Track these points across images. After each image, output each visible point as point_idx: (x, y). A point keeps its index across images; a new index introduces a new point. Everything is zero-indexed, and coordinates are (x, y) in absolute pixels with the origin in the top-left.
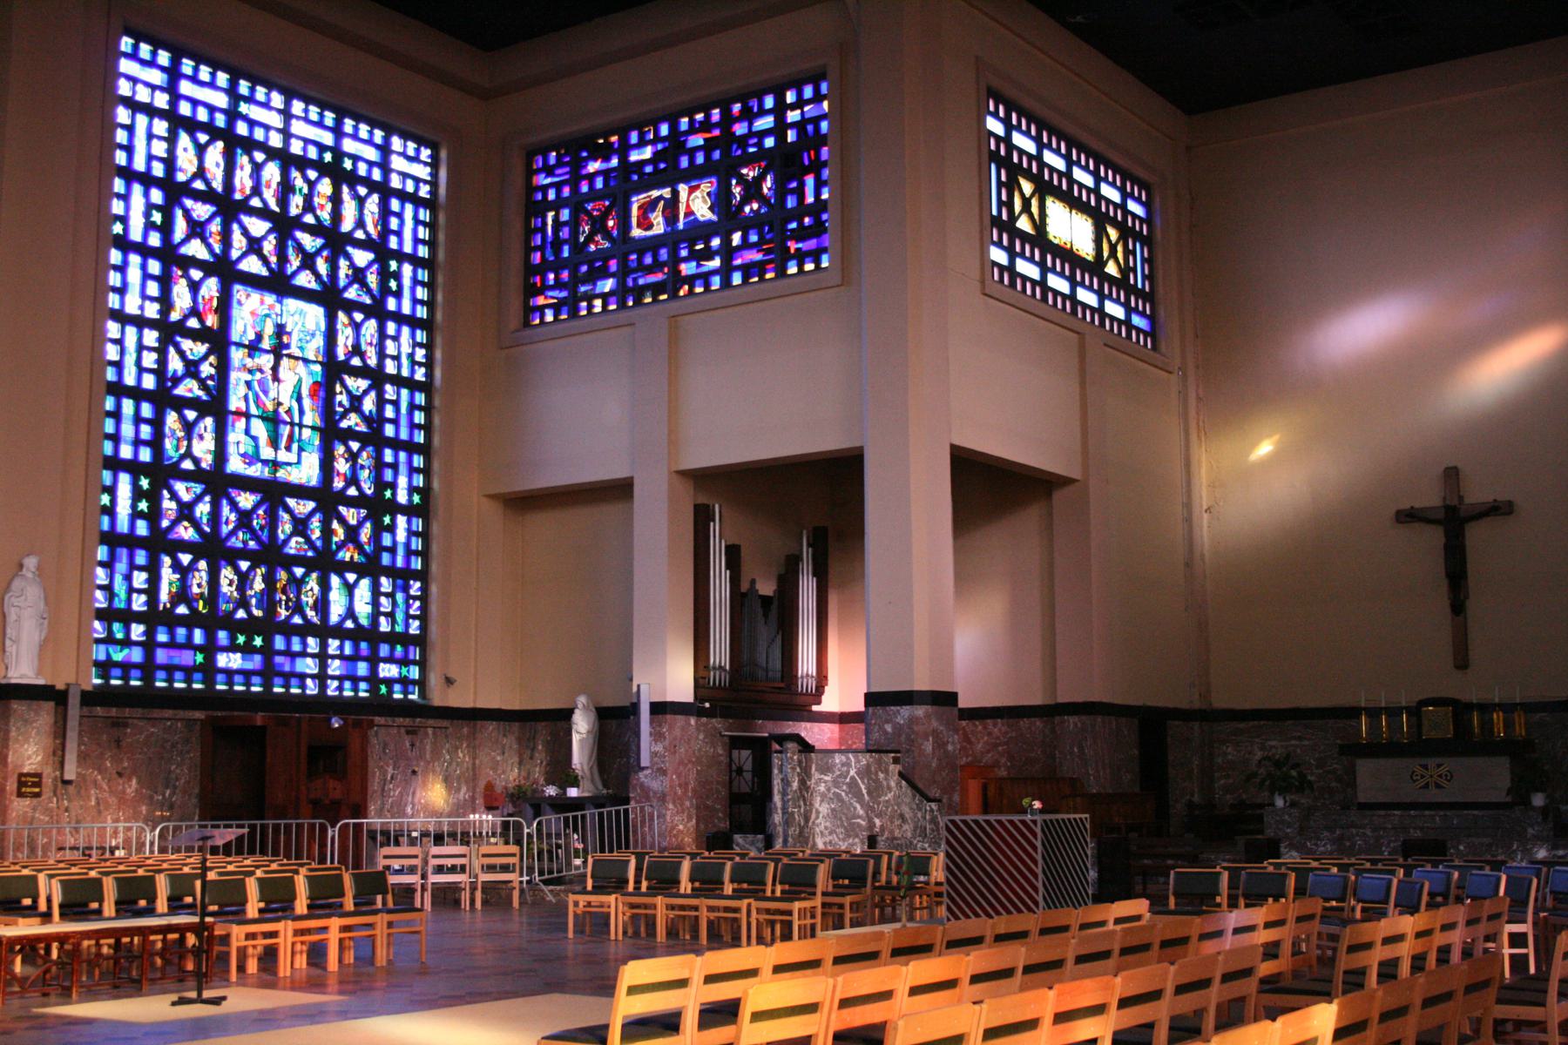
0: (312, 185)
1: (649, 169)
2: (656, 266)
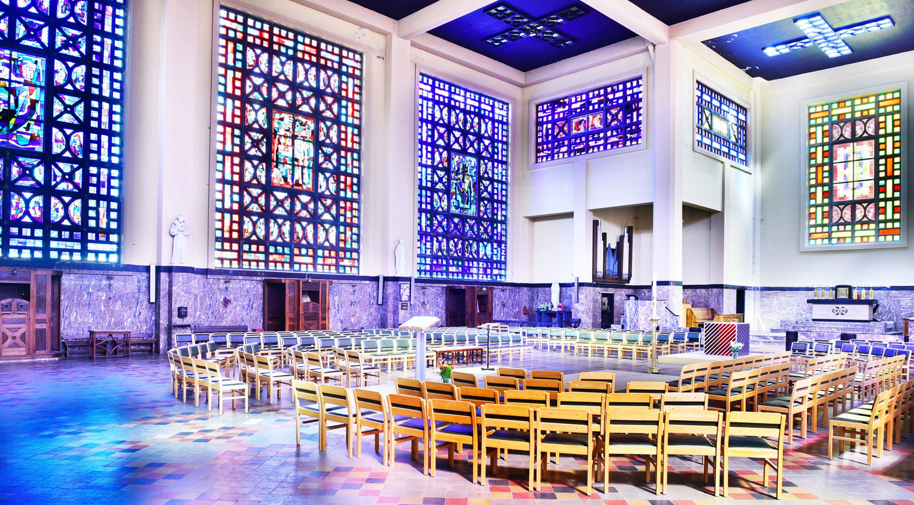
0: (472, 120)
1: (579, 110)
2: (581, 142)
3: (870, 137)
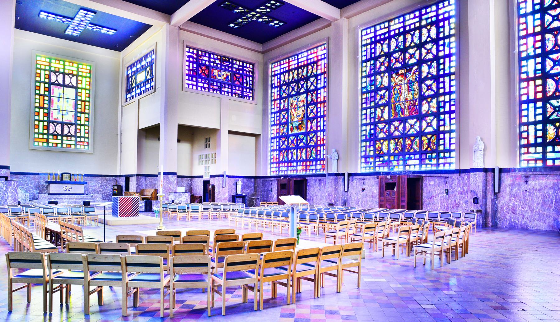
3: (73, 87)
